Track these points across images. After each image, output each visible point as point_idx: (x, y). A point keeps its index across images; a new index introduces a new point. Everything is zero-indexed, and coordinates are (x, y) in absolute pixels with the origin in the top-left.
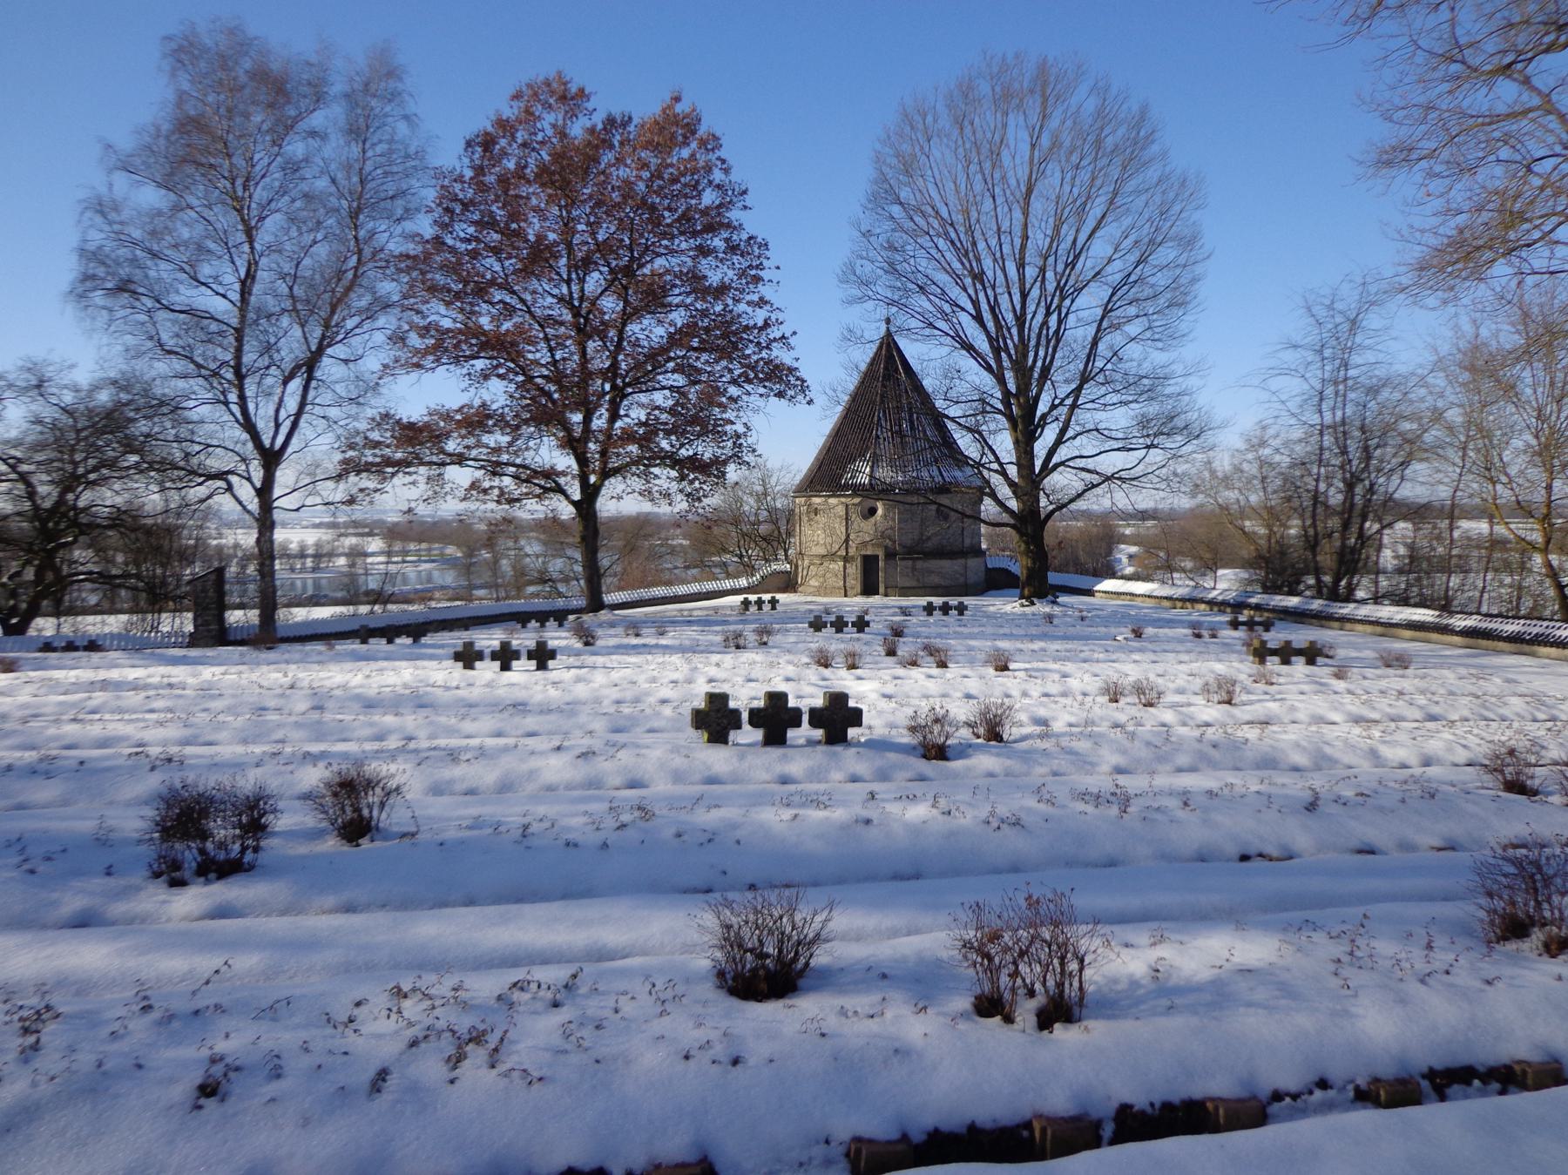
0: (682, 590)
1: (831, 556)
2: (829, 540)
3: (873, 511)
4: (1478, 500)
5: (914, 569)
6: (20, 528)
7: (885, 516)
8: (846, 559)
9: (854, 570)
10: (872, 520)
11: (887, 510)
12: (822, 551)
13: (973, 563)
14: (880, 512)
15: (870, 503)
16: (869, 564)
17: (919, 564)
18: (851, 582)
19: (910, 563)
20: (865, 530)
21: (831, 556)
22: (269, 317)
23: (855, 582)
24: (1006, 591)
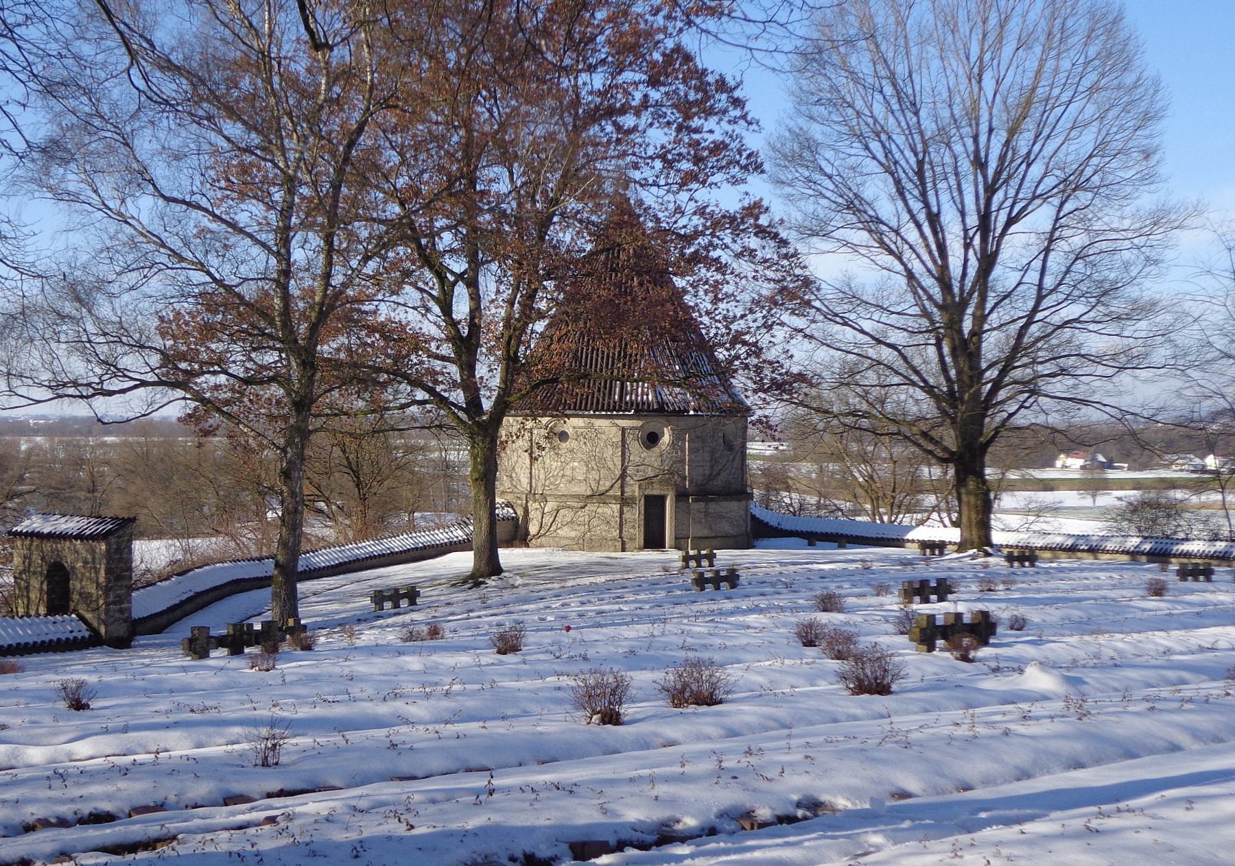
0: (424, 539)
1: (600, 497)
2: (594, 475)
3: (652, 439)
4: (504, 438)
5: (707, 514)
6: (139, 425)
7: (673, 445)
8: (625, 501)
9: (635, 515)
10: (656, 450)
11: (678, 438)
12: (583, 489)
13: (732, 507)
14: (666, 438)
15: (653, 426)
16: (654, 506)
17: (713, 507)
18: (628, 531)
19: (702, 505)
20: (648, 461)
21: (600, 497)
22: (686, 109)
23: (636, 532)
24: (766, 541)
